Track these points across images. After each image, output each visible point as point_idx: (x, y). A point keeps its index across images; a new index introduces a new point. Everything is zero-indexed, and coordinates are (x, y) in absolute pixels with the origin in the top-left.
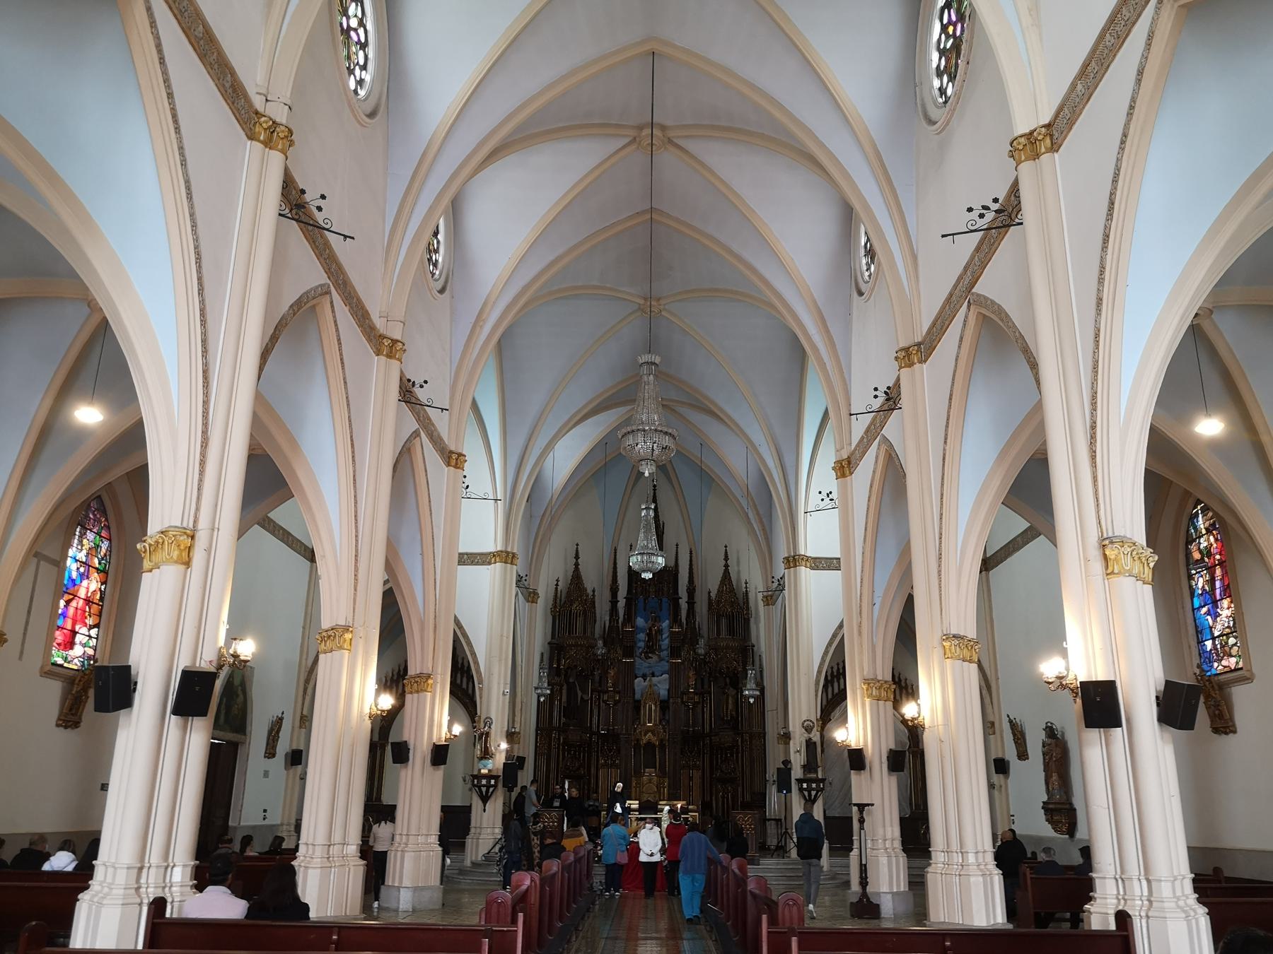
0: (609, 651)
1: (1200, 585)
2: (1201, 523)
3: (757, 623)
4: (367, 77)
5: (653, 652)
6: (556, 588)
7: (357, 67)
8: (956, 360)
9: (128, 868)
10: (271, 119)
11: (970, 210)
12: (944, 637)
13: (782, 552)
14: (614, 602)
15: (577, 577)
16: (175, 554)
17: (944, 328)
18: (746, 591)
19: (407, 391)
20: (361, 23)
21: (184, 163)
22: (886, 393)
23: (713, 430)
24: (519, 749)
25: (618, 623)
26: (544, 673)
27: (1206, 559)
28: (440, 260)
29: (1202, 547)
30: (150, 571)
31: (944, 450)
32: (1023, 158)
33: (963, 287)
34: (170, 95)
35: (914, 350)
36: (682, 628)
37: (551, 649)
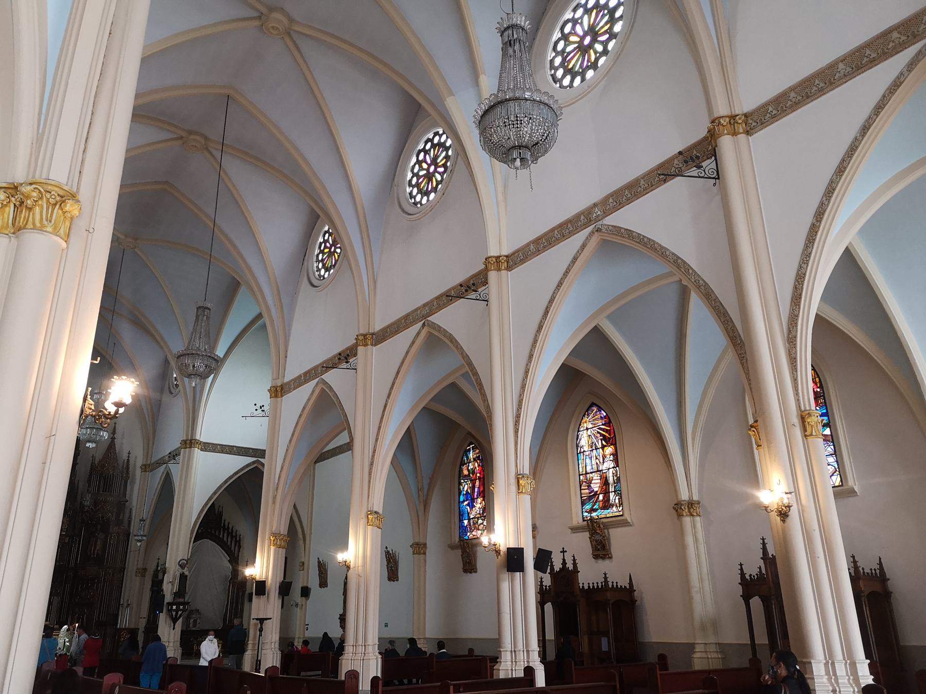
1: (465, 489)
2: (471, 455)
12: (369, 513)
27: (471, 475)
29: (469, 468)
32: (493, 268)
35: (369, 337)
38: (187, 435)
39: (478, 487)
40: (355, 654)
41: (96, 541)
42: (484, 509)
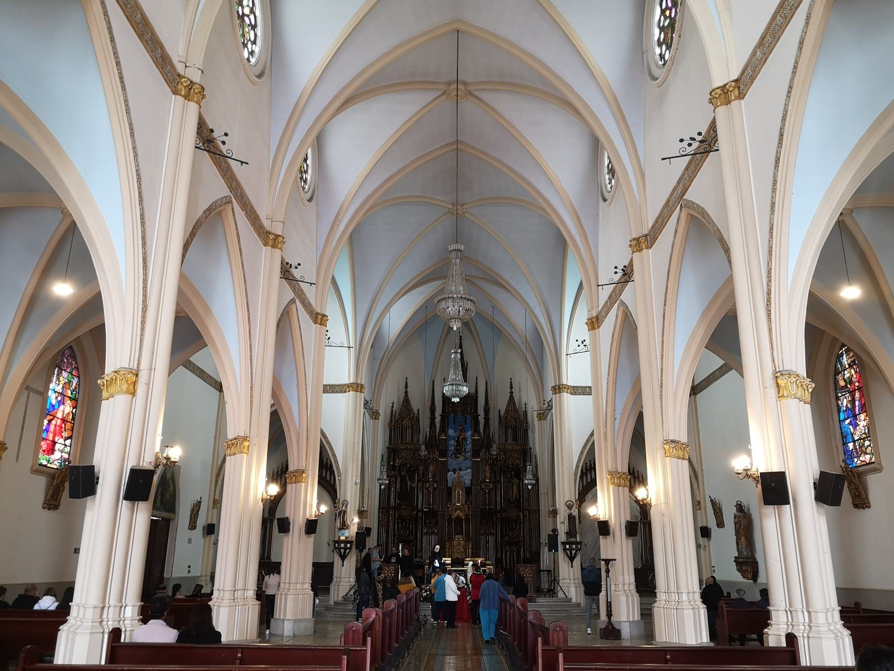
0: (430, 453)
1: (845, 404)
2: (845, 360)
3: (533, 433)
4: (256, 49)
5: (460, 454)
6: (392, 410)
7: (249, 42)
8: (672, 247)
9: (94, 608)
10: (189, 79)
11: (681, 140)
12: (665, 442)
13: (551, 383)
14: (433, 419)
15: (406, 400)
16: (125, 387)
17: (664, 224)
18: (526, 410)
19: (286, 271)
20: (252, 11)
21: (128, 111)
22: (623, 270)
23: (501, 296)
24: (367, 522)
25: (435, 433)
26: (384, 469)
27: (849, 386)
28: (309, 178)
29: (845, 377)
30: (108, 399)
31: (664, 310)
32: (719, 104)
33: (677, 195)
34: (118, 64)
35: (642, 240)
36: (481, 436)
37: (389, 451)
38: (555, 382)
39: (859, 400)
40: (678, 602)
41: (513, 486)
42: (868, 426)
